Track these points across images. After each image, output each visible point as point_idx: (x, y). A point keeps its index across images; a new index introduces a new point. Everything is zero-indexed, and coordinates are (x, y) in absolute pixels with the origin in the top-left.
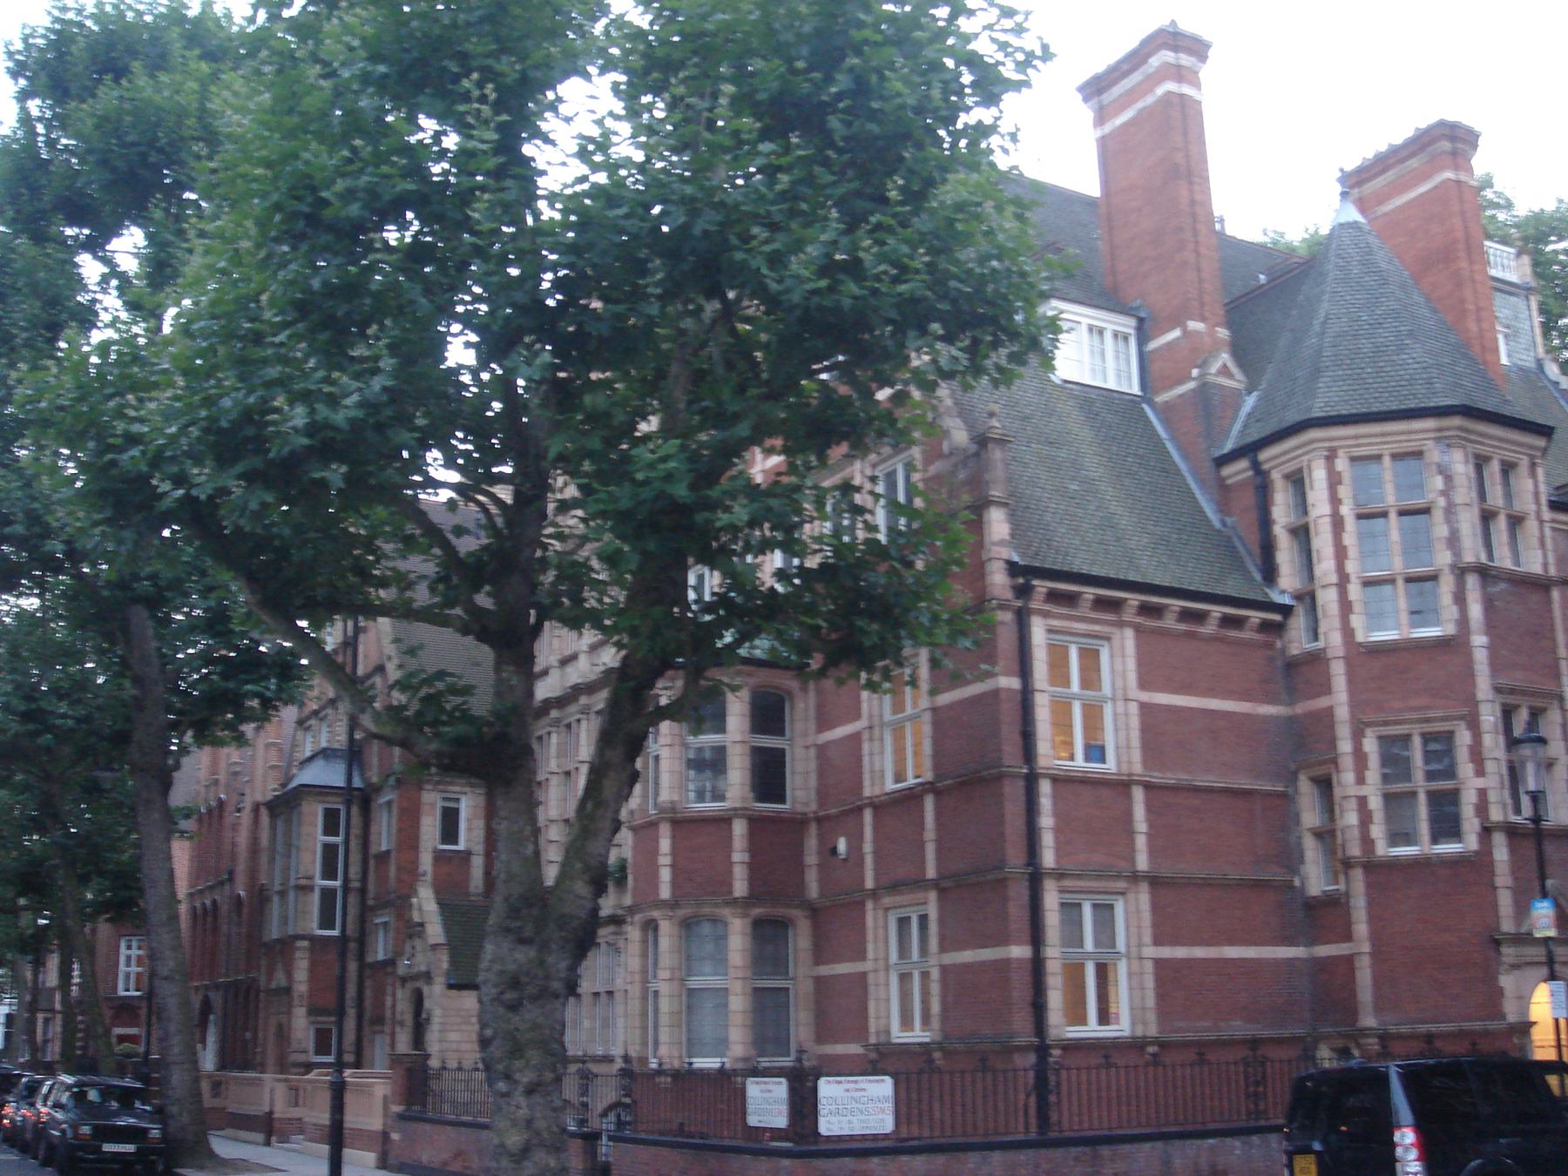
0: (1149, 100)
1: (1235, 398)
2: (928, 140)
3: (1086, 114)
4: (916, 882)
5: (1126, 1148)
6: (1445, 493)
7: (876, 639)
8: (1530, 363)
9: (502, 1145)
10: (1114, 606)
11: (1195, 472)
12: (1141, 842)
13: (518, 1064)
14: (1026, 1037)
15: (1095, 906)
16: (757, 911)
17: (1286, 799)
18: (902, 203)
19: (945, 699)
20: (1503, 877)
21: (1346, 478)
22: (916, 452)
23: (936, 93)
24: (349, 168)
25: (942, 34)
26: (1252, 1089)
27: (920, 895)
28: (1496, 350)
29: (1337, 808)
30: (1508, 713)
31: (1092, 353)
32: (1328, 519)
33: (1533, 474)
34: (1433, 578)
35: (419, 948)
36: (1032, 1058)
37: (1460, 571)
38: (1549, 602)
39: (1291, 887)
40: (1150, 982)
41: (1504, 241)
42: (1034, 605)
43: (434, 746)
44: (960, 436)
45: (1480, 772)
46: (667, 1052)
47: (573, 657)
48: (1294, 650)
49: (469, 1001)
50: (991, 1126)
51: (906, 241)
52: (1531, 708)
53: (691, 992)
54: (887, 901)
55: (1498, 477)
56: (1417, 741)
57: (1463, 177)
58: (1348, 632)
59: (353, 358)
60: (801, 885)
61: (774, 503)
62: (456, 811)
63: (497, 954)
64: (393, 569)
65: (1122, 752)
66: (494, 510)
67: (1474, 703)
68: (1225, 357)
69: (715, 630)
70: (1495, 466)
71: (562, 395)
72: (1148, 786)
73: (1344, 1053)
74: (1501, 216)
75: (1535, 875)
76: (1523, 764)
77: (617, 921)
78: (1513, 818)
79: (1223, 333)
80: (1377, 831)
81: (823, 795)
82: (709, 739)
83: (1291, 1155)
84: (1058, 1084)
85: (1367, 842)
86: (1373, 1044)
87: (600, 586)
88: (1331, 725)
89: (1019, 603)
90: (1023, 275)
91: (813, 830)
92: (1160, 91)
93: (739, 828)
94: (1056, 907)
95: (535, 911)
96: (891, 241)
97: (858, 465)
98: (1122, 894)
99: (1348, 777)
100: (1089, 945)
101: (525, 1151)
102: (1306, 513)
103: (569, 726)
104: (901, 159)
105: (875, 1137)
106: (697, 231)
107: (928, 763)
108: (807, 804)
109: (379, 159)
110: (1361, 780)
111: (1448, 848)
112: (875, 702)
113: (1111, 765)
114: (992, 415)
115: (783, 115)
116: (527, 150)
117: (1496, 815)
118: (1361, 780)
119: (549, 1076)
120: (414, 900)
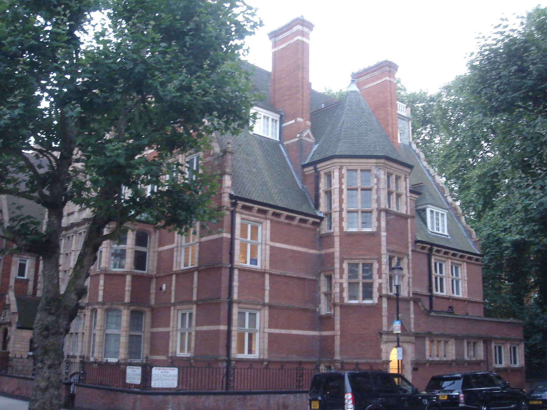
0: (292, 41)
1: (311, 146)
2: (219, 49)
3: (270, 43)
4: (189, 302)
5: (255, 396)
6: (376, 184)
7: (184, 217)
8: (407, 143)
9: (38, 386)
10: (265, 212)
11: (295, 169)
12: (267, 293)
13: (46, 357)
14: (223, 357)
15: (250, 314)
16: (132, 308)
17: (316, 282)
18: (208, 69)
19: (204, 239)
20: (385, 313)
21: (345, 176)
22: (201, 154)
23: (223, 33)
24: (14, 33)
25: (228, 12)
26: (298, 378)
27: (190, 306)
28: (397, 138)
29: (333, 286)
30: (391, 259)
31: (264, 125)
32: (338, 189)
33: (405, 180)
34: (371, 212)
35: (7, 313)
36: (225, 364)
37: (380, 211)
38: (407, 223)
39: (315, 311)
40: (266, 341)
41: (402, 102)
42: (237, 210)
43: (24, 242)
44: (217, 149)
45: (380, 277)
46: (97, 355)
47: (72, 213)
48: (323, 232)
49: (27, 334)
50: (210, 386)
51: (208, 82)
52: (398, 257)
53: (107, 335)
54: (178, 307)
55: (394, 180)
56: (361, 266)
57: (392, 80)
58: (341, 228)
59: (8, 102)
60: (149, 300)
61: (154, 168)
63: (41, 318)
64: (13, 177)
65: (263, 262)
66: (52, 159)
67: (380, 254)
68: (309, 131)
69: (128, 209)
70: (394, 177)
71: (83, 123)
72: (271, 274)
73: (329, 368)
74: (402, 93)
75: (395, 312)
76: (394, 276)
77: (82, 308)
78: (390, 294)
79: (309, 123)
80: (345, 294)
81: (158, 269)
82: (122, 246)
83: (311, 401)
84: (234, 374)
85: (342, 298)
86: (339, 365)
87: (88, 190)
88: (333, 258)
89: (232, 209)
90: (246, 98)
91: (154, 281)
92: (296, 39)
93: (128, 278)
94: (237, 313)
95: (56, 303)
96: (203, 82)
97: (181, 155)
98: (260, 310)
99: (337, 276)
100: (247, 327)
101: (47, 388)
102: (331, 186)
103: (69, 237)
104: (209, 54)
105: (170, 389)
106: (136, 71)
107: (196, 261)
108: (153, 271)
109: (24, 31)
110: (341, 277)
111: (368, 302)
112: (435, 348)
113: (259, 266)
114: (229, 143)
115: (170, 34)
116: (77, 33)
117: (384, 292)
118: (341, 277)
119: (57, 362)
120: (7, 296)
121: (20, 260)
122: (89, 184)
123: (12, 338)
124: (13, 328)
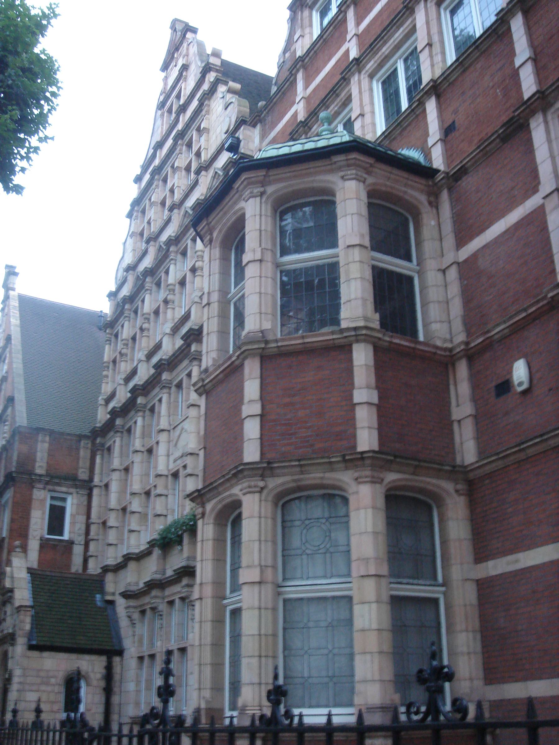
60: (450, 446)
62: (62, 510)
81: (473, 318)
91: (462, 370)
93: (362, 356)
103: (152, 410)
120: (8, 569)
121: (52, 498)
122: (204, 366)
123: (17, 672)
124: (19, 648)
